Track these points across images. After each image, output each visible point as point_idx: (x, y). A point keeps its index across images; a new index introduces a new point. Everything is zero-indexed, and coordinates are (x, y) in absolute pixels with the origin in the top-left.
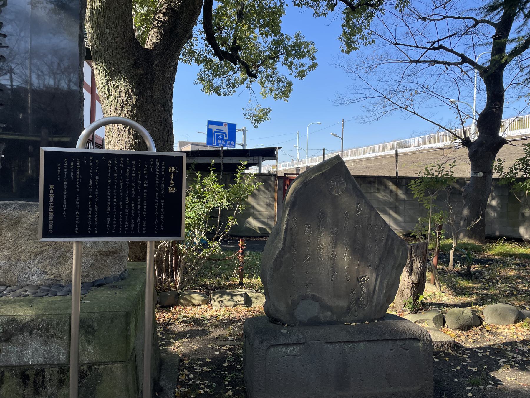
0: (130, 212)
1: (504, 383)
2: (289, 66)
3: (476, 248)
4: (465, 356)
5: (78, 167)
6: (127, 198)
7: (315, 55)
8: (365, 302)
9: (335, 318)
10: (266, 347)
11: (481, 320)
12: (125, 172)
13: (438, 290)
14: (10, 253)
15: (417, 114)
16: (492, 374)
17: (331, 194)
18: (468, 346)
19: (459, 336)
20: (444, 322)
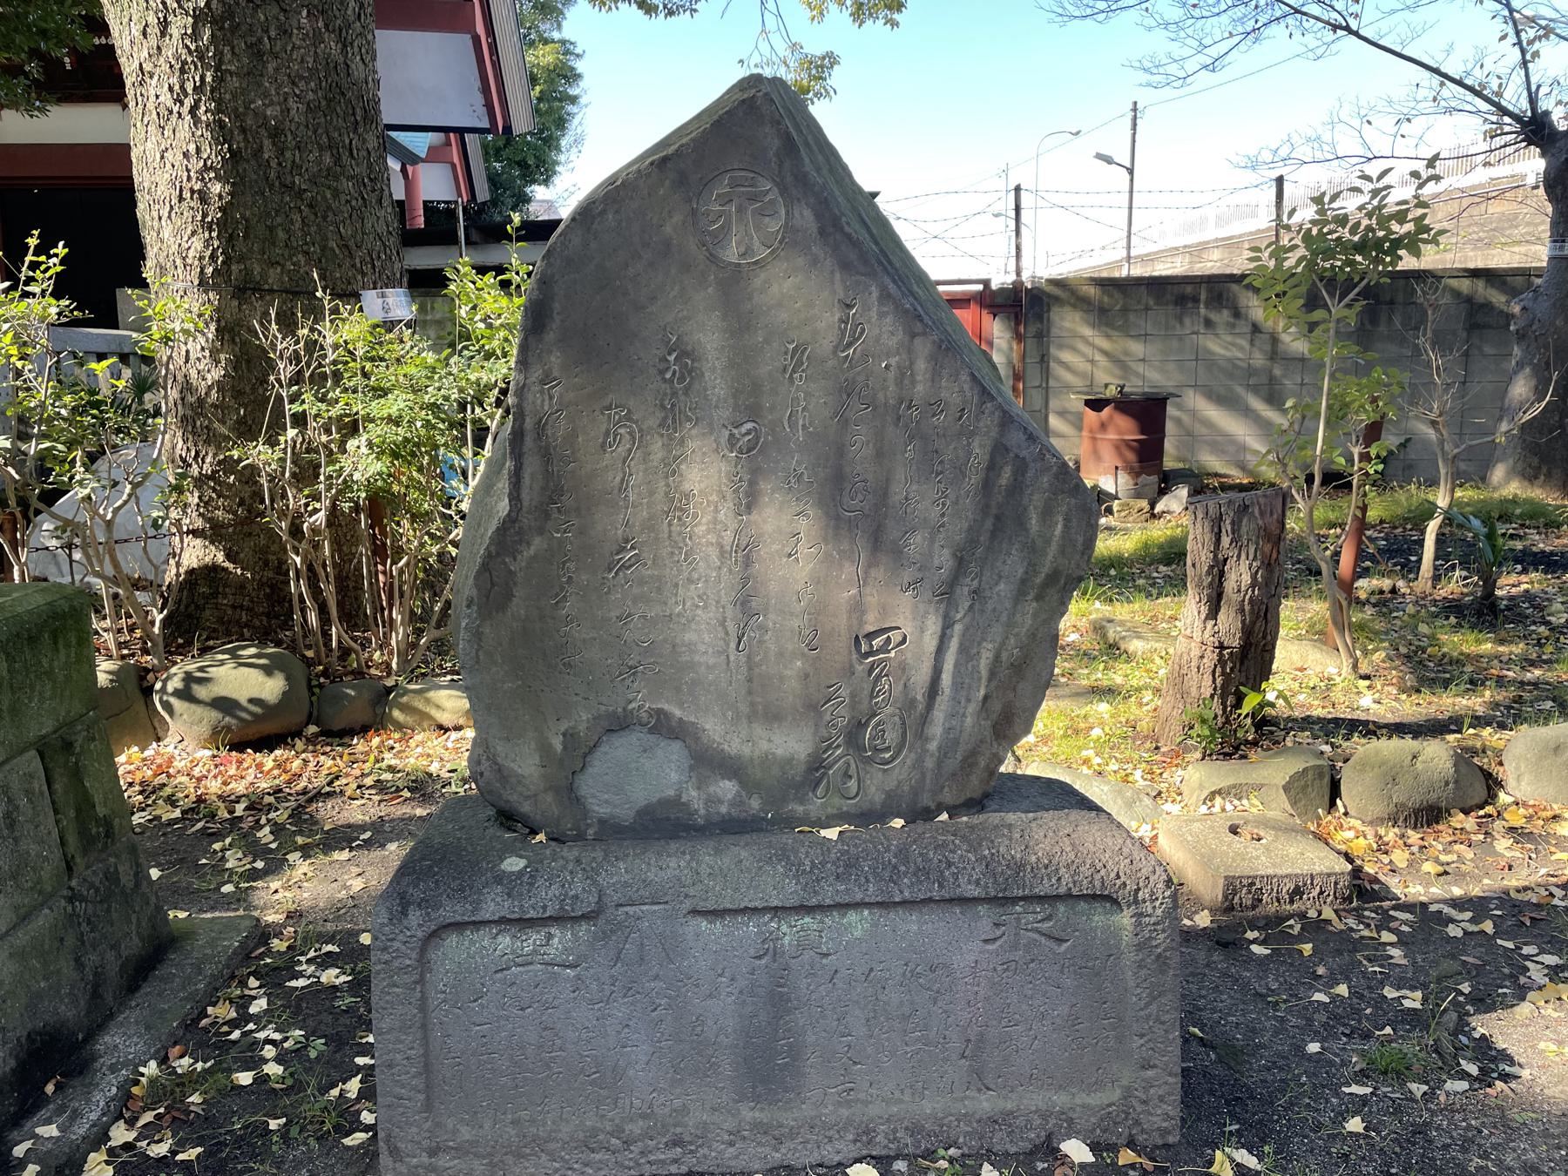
1: (1525, 1074)
3: (1543, 514)
4: (1386, 937)
8: (891, 737)
9: (755, 804)
10: (420, 934)
11: (1492, 784)
13: (1346, 668)
15: (1356, 34)
16: (1482, 1025)
17: (713, 259)
18: (1416, 891)
19: (1383, 848)
20: (1335, 791)
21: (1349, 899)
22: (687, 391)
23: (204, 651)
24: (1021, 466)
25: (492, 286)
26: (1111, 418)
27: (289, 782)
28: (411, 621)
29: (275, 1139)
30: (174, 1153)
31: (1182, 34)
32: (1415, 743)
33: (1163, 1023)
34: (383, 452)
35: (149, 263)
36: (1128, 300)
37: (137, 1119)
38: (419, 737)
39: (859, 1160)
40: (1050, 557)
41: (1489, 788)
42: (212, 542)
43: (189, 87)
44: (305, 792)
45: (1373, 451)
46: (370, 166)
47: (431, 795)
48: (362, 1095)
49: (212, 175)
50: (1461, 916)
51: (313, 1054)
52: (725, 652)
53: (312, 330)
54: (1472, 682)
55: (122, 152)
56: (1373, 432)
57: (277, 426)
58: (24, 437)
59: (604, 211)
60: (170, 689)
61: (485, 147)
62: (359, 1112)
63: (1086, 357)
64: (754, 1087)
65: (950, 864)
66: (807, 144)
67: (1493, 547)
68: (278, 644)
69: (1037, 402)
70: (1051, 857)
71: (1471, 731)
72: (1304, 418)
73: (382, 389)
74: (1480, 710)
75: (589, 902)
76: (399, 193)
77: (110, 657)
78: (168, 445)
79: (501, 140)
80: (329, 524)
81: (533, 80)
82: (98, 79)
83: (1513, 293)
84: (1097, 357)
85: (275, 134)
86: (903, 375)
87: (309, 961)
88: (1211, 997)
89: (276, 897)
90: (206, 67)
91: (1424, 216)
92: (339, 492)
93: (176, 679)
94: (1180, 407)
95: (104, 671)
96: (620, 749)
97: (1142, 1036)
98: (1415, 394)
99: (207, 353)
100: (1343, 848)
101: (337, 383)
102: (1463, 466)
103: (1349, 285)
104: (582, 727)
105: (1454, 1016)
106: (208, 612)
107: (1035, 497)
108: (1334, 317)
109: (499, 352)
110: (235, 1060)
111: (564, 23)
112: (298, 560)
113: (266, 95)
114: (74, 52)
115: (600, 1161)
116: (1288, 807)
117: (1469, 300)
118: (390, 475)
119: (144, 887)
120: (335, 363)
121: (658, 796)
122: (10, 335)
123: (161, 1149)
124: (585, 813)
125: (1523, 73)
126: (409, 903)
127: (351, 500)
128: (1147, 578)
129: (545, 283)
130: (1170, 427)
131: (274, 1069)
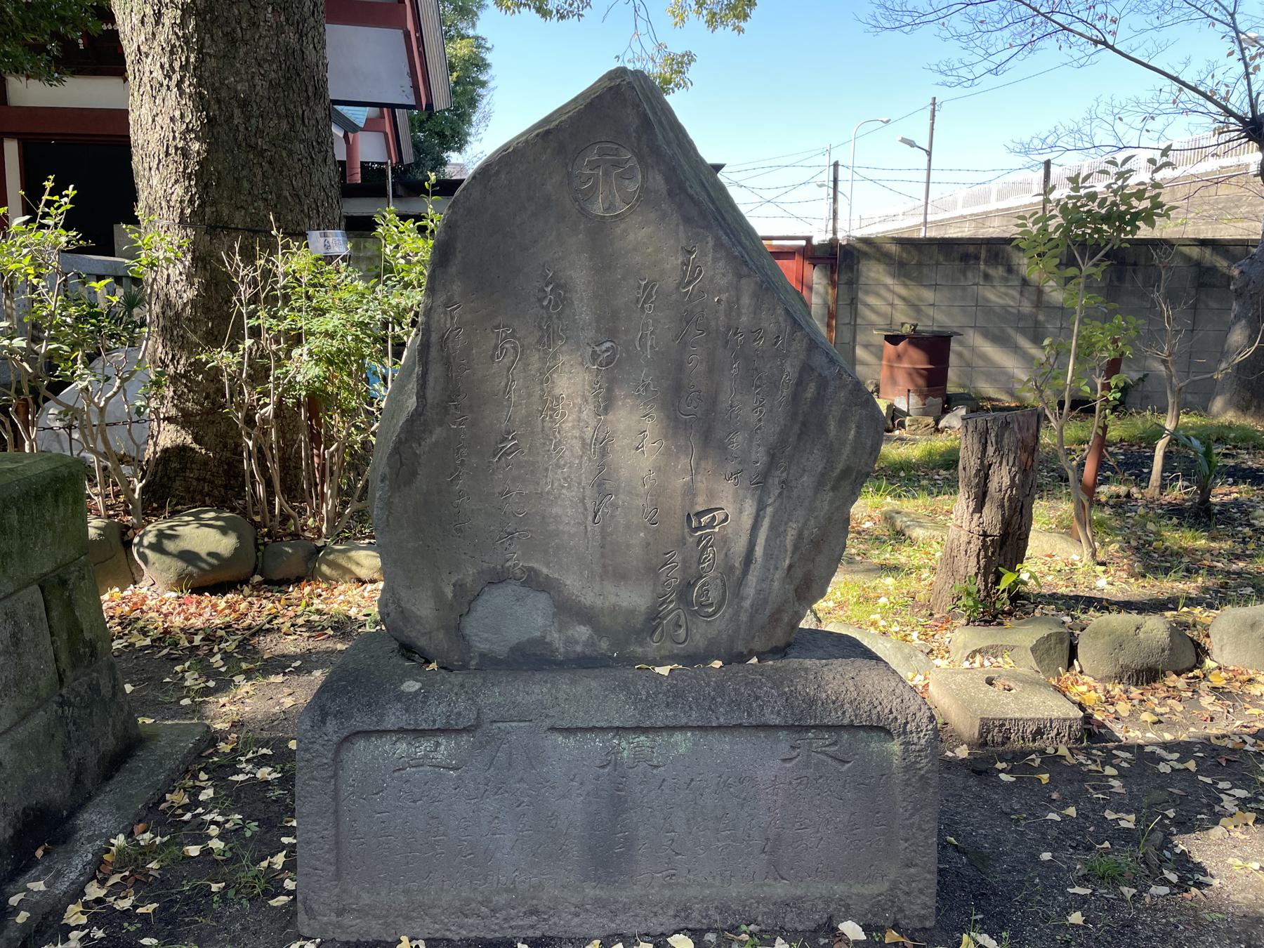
1: (1216, 883)
3: (1252, 438)
4: (1109, 771)
8: (714, 595)
9: (604, 645)
10: (335, 738)
11: (1200, 652)
15: (1112, 48)
16: (1182, 843)
17: (584, 212)
18: (1134, 735)
19: (1110, 700)
20: (1073, 653)
21: (1080, 740)
22: (559, 315)
23: (173, 513)
24: (823, 383)
25: (411, 230)
26: (905, 350)
27: (237, 620)
28: (338, 495)
29: (215, 898)
30: (135, 907)
31: (972, 44)
32: (1139, 617)
33: (924, 830)
34: (320, 360)
35: (140, 205)
36: (923, 256)
37: (106, 880)
38: (342, 588)
39: (677, 932)
40: (844, 457)
41: (1198, 655)
42: (183, 428)
43: (177, 65)
44: (249, 628)
45: (1113, 382)
46: (318, 132)
47: (349, 634)
48: (286, 867)
49: (193, 136)
50: (1170, 757)
51: (248, 834)
52: (584, 523)
53: (267, 261)
54: (1188, 570)
55: (121, 116)
56: (1113, 367)
57: (238, 337)
58: (36, 340)
59: (498, 172)
60: (146, 542)
61: (411, 119)
62: (283, 880)
63: (888, 301)
64: (596, 870)
65: (757, 698)
66: (660, 123)
67: (1209, 463)
68: (233, 510)
69: (847, 337)
70: (838, 694)
71: (1185, 609)
72: (1058, 354)
73: (321, 310)
74: (1194, 593)
75: (469, 718)
76: (340, 154)
77: (99, 516)
78: (150, 349)
79: (425, 114)
80: (276, 416)
81: (452, 68)
82: (105, 57)
83: (1233, 259)
84: (897, 301)
85: (244, 104)
86: (731, 308)
87: (248, 761)
88: (966, 814)
89: (224, 709)
90: (190, 50)
91: (1159, 195)
92: (285, 390)
93: (150, 535)
94: (961, 343)
95: (94, 526)
96: (498, 598)
97: (906, 840)
98: (1153, 337)
99: (184, 277)
100: (1077, 699)
101: (286, 303)
102: (1189, 398)
103: (1097, 248)
104: (469, 580)
105: (1160, 835)
106: (178, 483)
107: (834, 408)
108: (1084, 274)
109: (415, 283)
110: (186, 836)
111: (478, 23)
112: (250, 443)
113: (237, 73)
114: (86, 36)
115: (472, 925)
116: (1034, 664)
117: (1198, 264)
118: (325, 378)
119: (120, 697)
120: (284, 287)
121: (527, 637)
122: (29, 258)
123: (126, 904)
124: (469, 647)
125: (1245, 82)
126: (327, 714)
127: (294, 397)
128: (931, 479)
129: (449, 226)
130: (953, 359)
131: (216, 844)
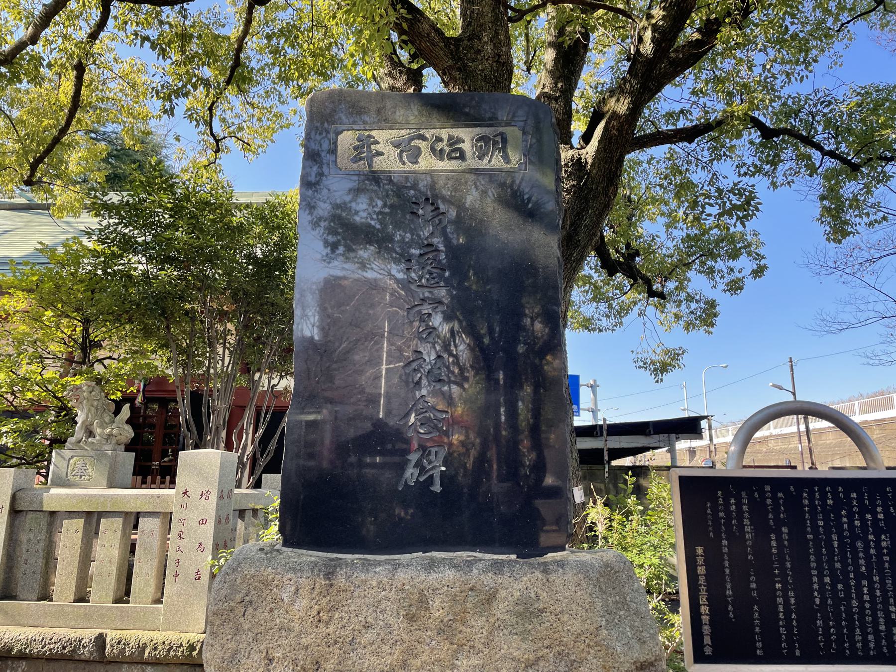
0: (861, 607)
2: (708, 274)
5: (745, 508)
6: (852, 576)
7: (761, 251)
12: (839, 517)
14: (481, 663)
